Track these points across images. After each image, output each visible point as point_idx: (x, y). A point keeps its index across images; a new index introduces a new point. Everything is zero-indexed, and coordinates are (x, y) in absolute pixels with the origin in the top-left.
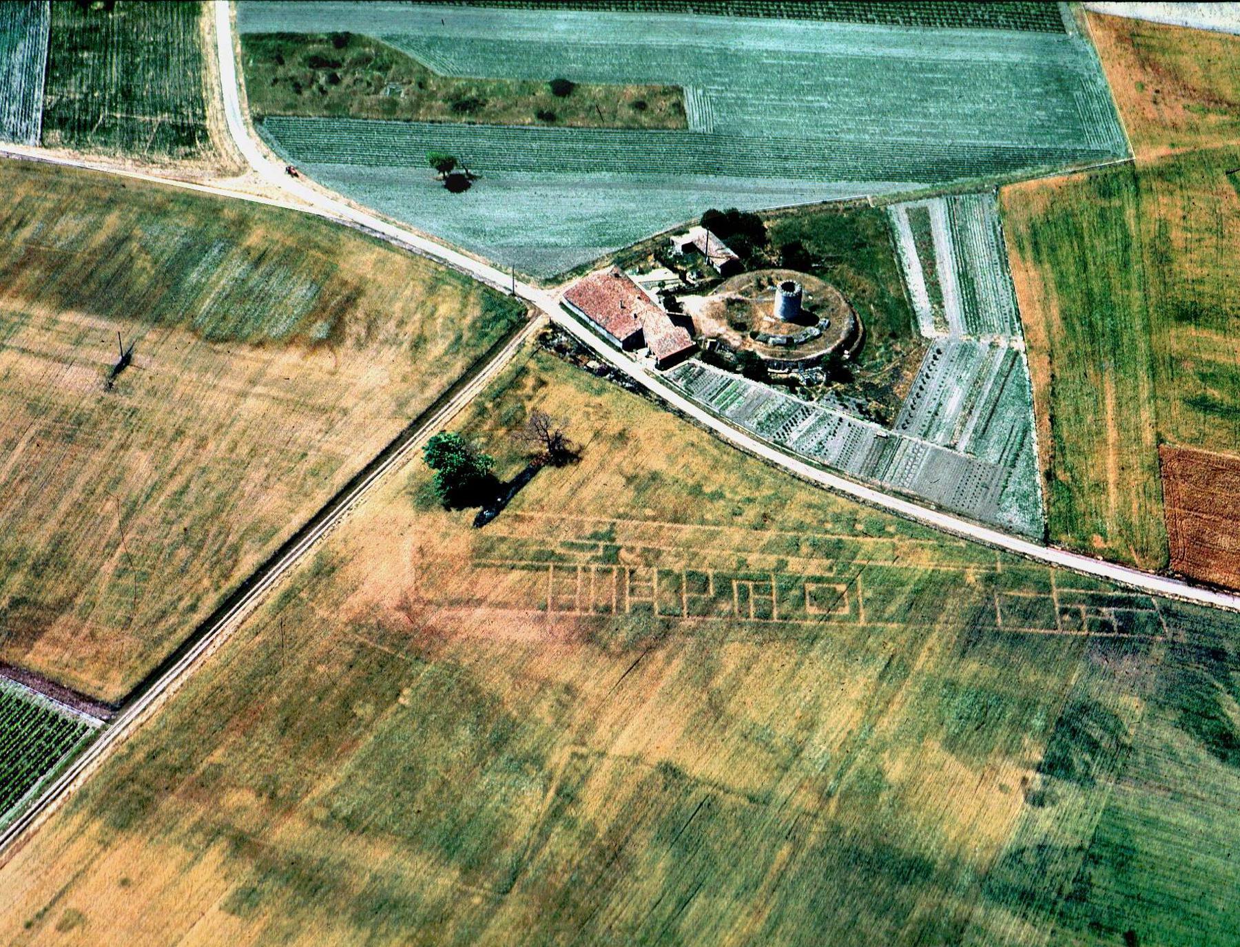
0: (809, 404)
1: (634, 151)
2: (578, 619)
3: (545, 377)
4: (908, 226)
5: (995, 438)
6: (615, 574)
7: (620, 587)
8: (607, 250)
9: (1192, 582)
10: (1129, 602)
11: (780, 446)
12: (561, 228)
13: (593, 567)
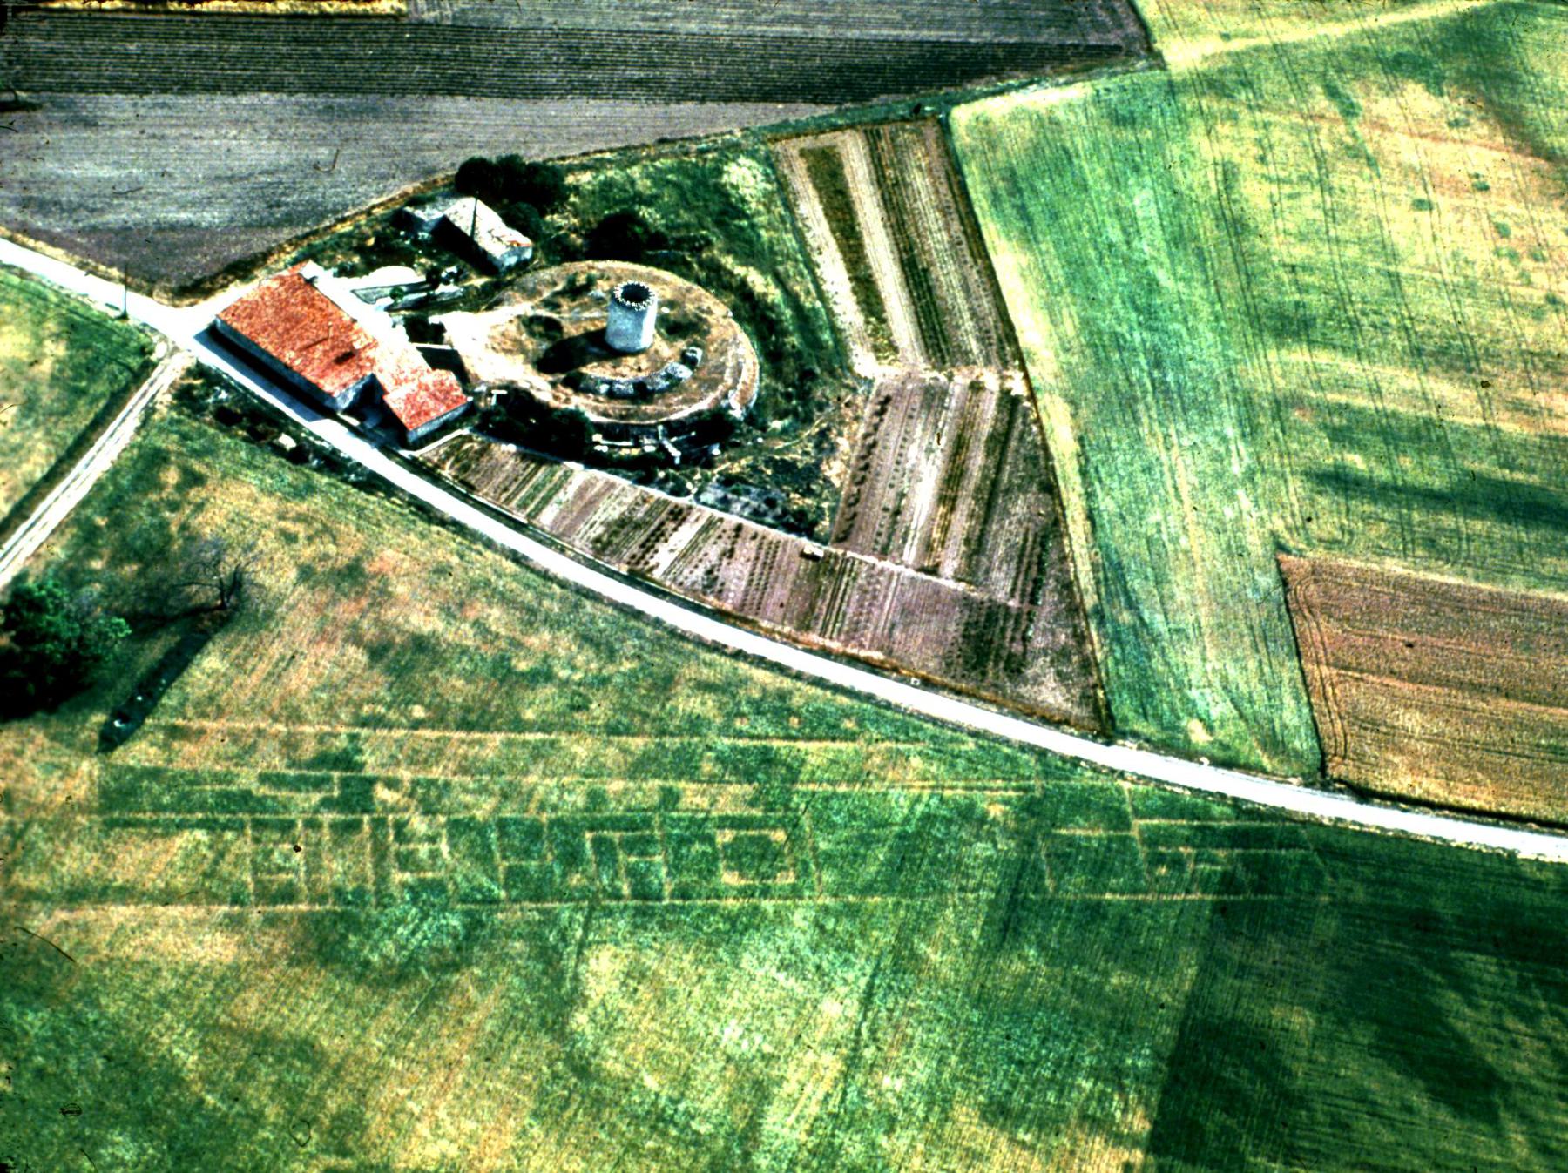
0: (683, 501)
1: (316, 56)
2: (303, 917)
3: (198, 467)
4: (806, 179)
5: (1001, 551)
6: (366, 828)
7: (380, 853)
8: (286, 233)
9: (1363, 794)
10: (1264, 838)
11: (637, 578)
12: (197, 193)
13: (327, 817)
